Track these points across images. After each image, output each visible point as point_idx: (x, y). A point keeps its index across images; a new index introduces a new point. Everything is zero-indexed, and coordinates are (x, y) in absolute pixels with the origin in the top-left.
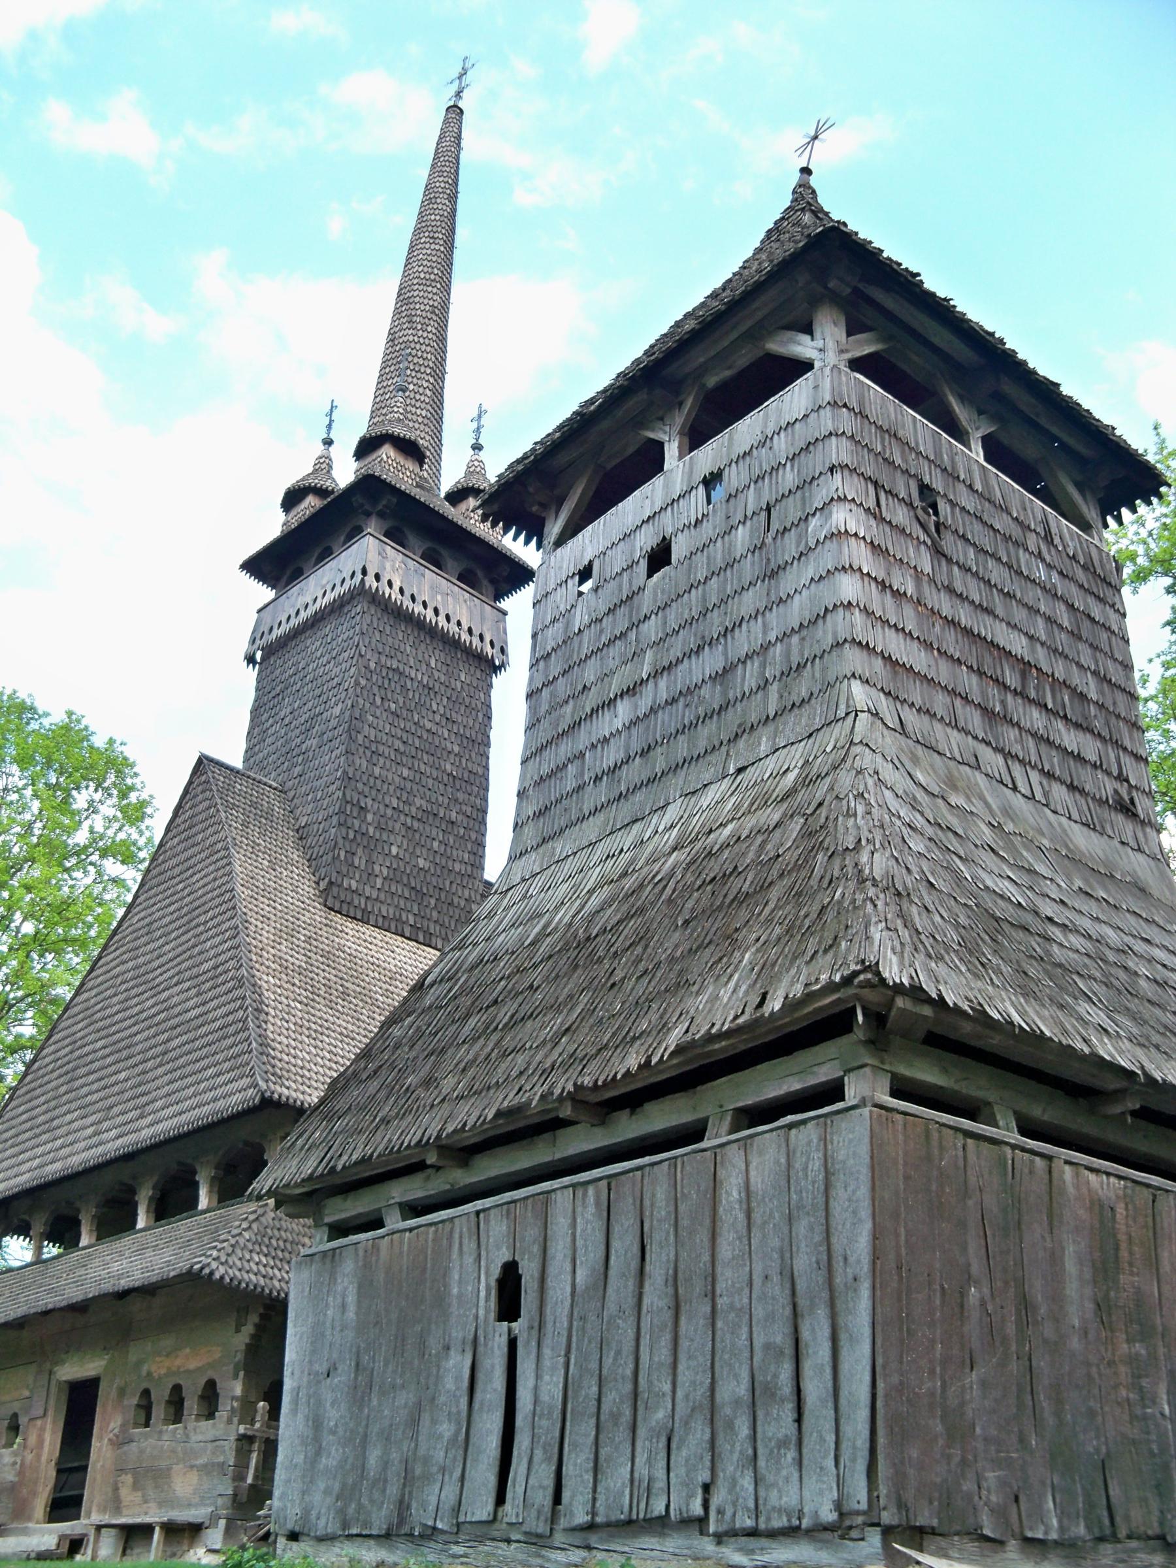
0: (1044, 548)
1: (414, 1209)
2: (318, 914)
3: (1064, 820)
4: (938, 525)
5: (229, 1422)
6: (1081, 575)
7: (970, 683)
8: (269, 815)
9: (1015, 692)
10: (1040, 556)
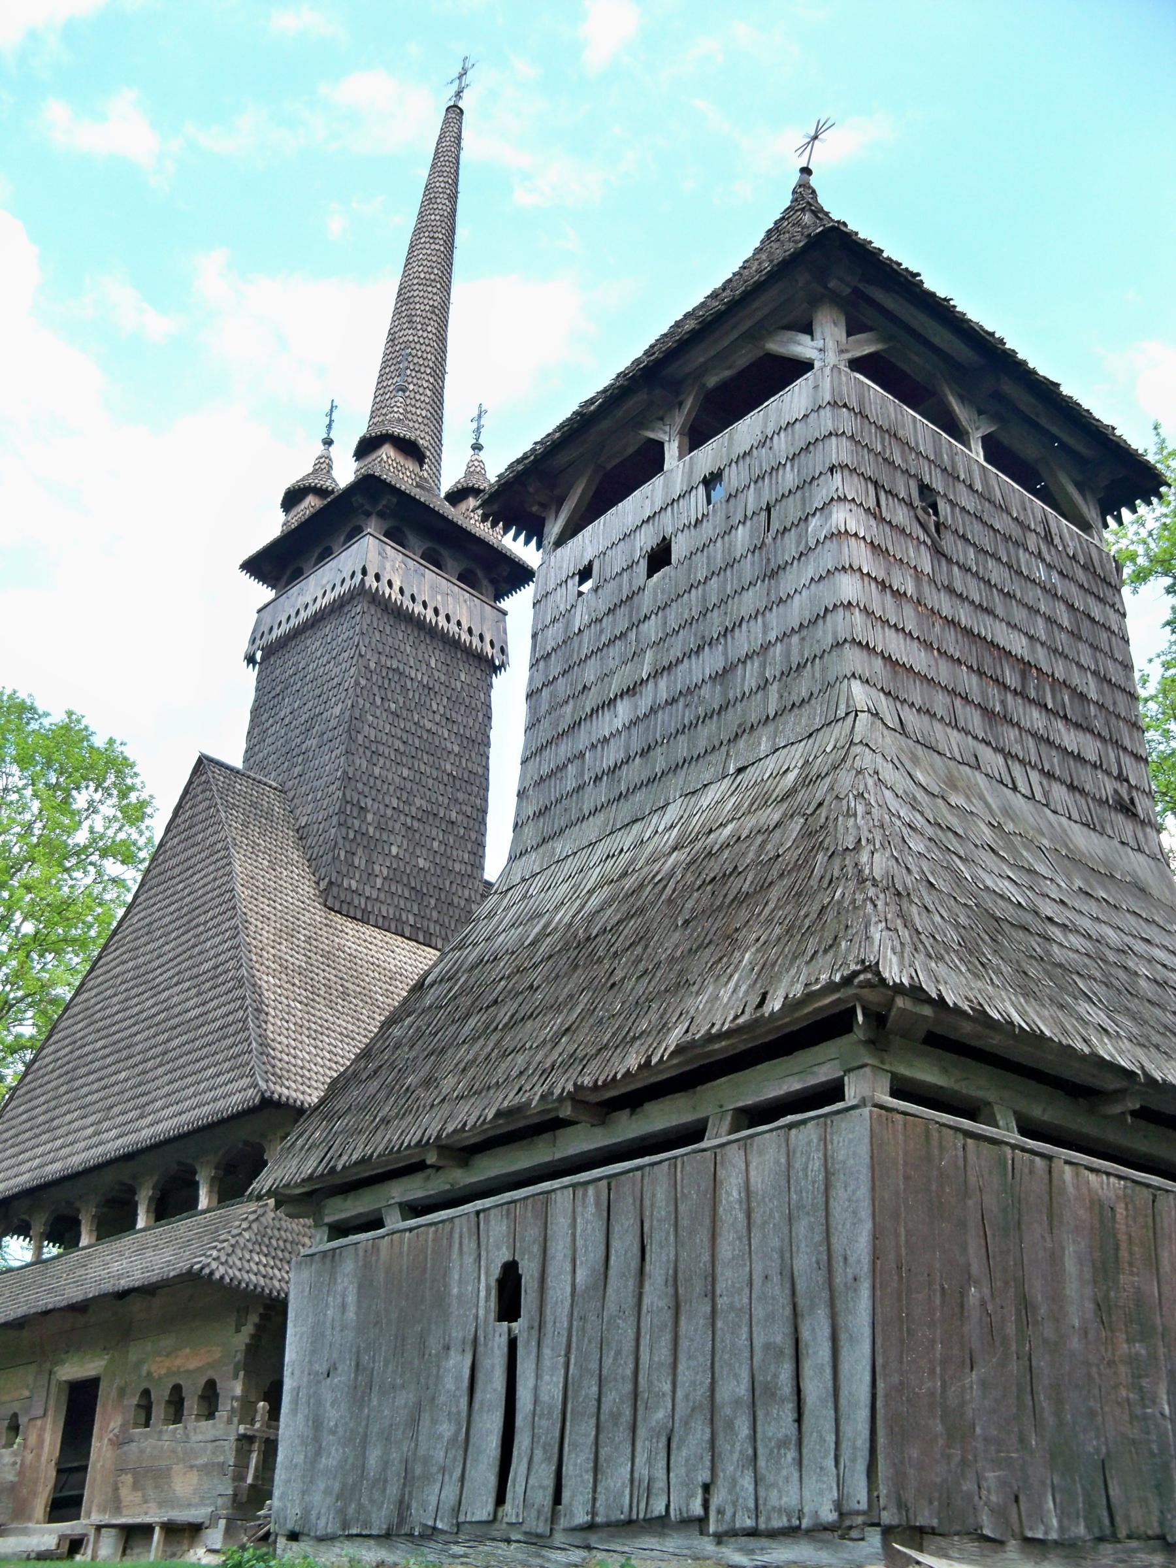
0: (1044, 548)
1: (414, 1209)
2: (318, 914)
3: (1064, 820)
4: (938, 525)
5: (229, 1422)
6: (1081, 575)
7: (970, 683)
8: (269, 815)
9: (1015, 692)
10: (1040, 556)
